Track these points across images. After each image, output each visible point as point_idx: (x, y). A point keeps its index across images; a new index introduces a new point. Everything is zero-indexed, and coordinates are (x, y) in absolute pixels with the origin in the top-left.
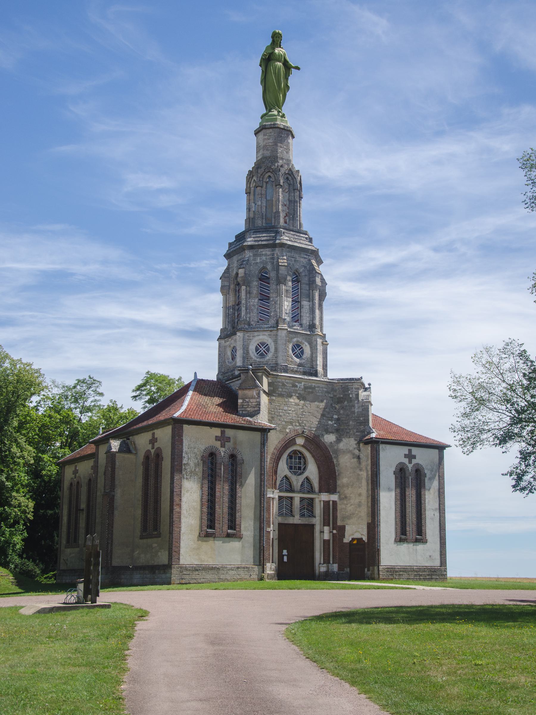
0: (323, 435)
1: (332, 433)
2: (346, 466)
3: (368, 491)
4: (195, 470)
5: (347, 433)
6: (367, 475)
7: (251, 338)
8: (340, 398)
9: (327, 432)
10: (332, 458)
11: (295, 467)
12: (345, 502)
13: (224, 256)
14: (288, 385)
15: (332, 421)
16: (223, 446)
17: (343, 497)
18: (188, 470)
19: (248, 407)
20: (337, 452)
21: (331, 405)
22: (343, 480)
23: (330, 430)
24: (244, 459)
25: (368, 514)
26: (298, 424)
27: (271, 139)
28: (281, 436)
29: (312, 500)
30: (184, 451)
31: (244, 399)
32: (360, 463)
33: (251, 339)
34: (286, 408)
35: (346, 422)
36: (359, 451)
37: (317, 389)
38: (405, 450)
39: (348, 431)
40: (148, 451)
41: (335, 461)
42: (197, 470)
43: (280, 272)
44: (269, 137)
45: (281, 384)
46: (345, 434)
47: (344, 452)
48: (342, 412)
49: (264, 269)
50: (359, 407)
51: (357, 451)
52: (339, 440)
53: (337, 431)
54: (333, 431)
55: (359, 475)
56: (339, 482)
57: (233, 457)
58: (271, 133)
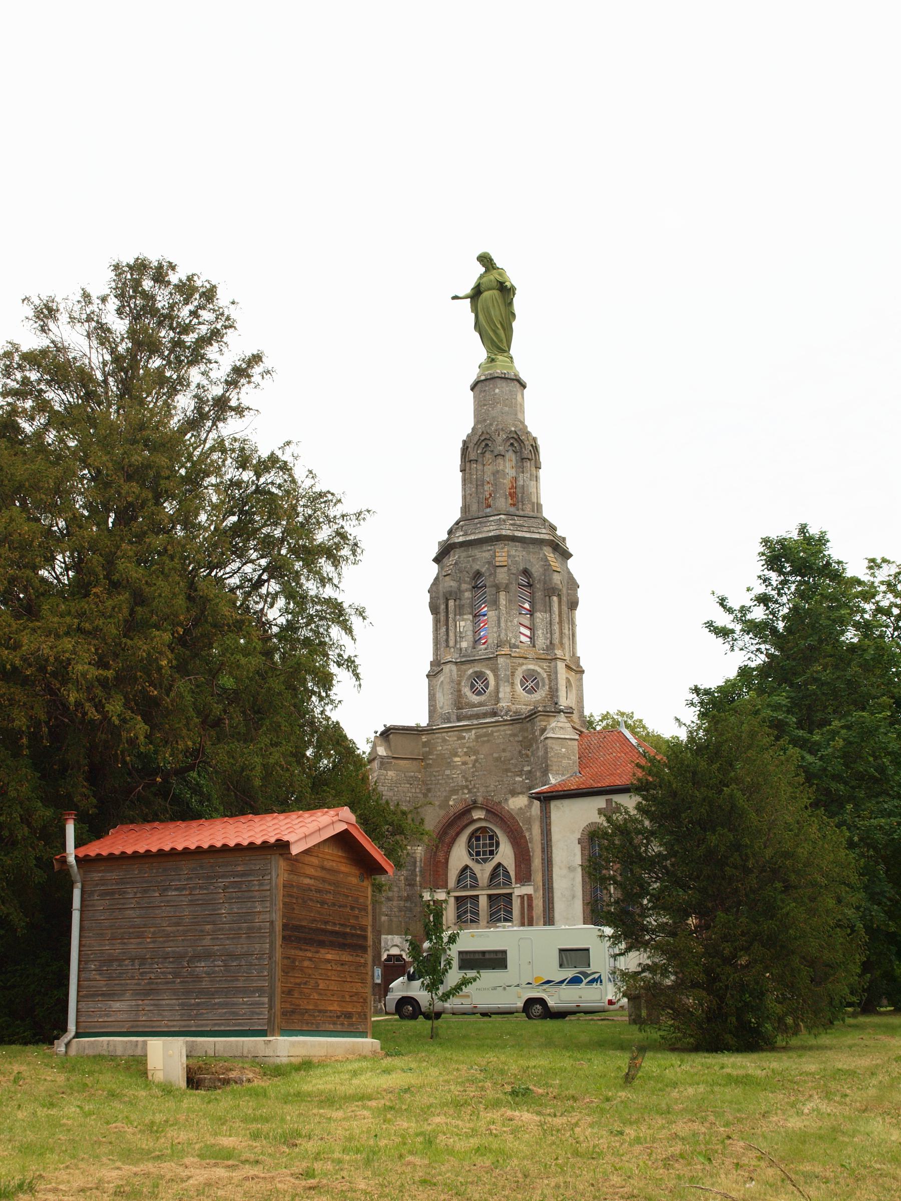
0: (506, 800)
1: (522, 793)
9: (514, 793)
10: (522, 832)
13: (571, 555)
15: (520, 776)
21: (520, 752)
26: (466, 791)
28: (442, 813)
29: (511, 894)
34: (448, 772)
37: (495, 734)
38: (600, 802)
41: (527, 834)
45: (440, 741)
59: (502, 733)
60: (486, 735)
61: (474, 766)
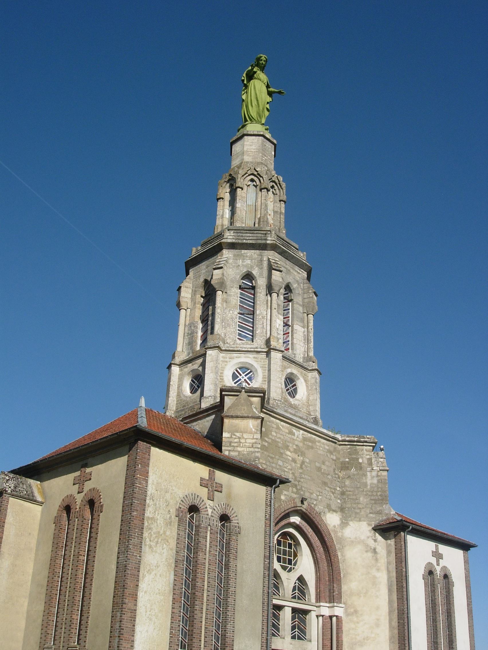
2: (356, 563)
3: (390, 602)
4: (165, 533)
5: (356, 513)
6: (389, 578)
7: (228, 360)
8: (344, 463)
9: (330, 509)
11: (285, 559)
12: (355, 619)
14: (283, 429)
16: (211, 498)
17: (352, 610)
18: (154, 530)
19: (239, 446)
20: (341, 540)
22: (351, 584)
23: (333, 507)
24: (241, 525)
25: (391, 638)
26: (295, 490)
27: (254, 146)
29: (306, 612)
30: (149, 493)
31: (233, 433)
32: (377, 560)
33: (226, 362)
34: (280, 463)
35: (354, 497)
36: (375, 541)
39: (358, 511)
40: (71, 497)
41: (339, 554)
42: (168, 533)
43: (273, 277)
44: (251, 144)
45: (275, 426)
46: (354, 515)
47: (352, 542)
48: (347, 482)
49: (248, 276)
50: (373, 477)
51: (373, 542)
52: (344, 524)
53: (342, 509)
54: (337, 509)
55: (375, 577)
56: (344, 588)
57: (224, 518)
58: (253, 140)
59: (322, 446)
60: (310, 440)
61: (301, 467)
